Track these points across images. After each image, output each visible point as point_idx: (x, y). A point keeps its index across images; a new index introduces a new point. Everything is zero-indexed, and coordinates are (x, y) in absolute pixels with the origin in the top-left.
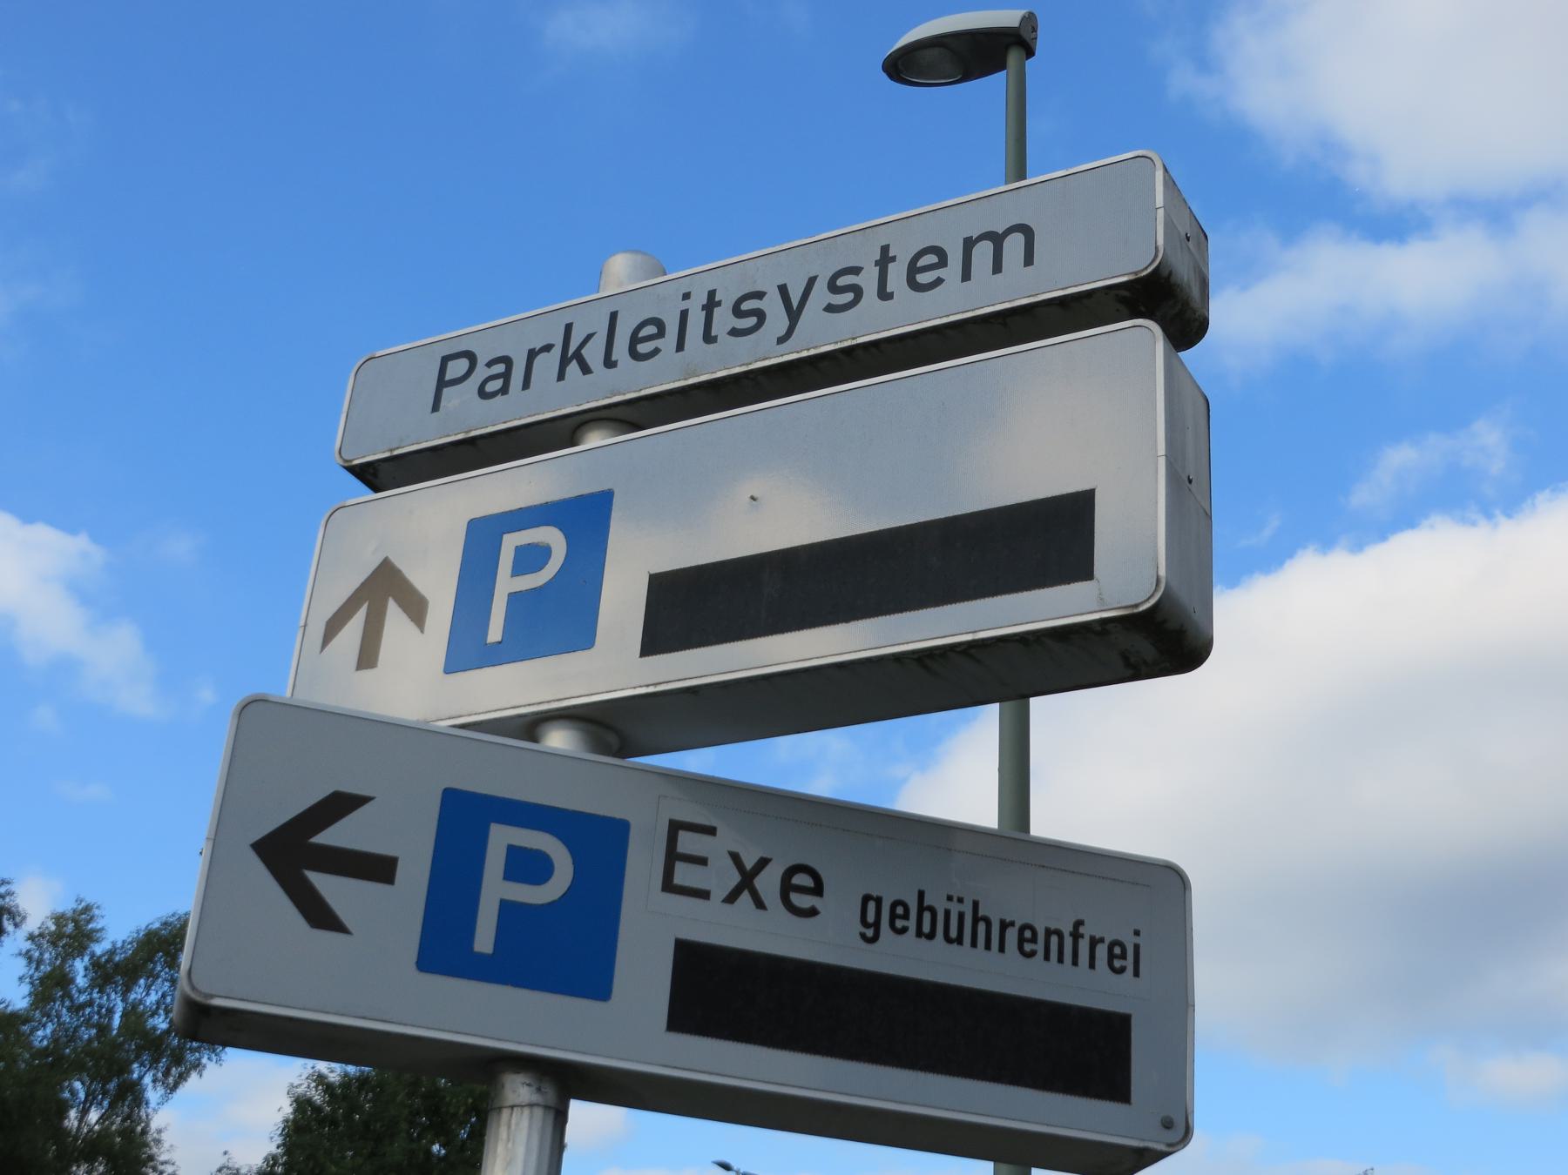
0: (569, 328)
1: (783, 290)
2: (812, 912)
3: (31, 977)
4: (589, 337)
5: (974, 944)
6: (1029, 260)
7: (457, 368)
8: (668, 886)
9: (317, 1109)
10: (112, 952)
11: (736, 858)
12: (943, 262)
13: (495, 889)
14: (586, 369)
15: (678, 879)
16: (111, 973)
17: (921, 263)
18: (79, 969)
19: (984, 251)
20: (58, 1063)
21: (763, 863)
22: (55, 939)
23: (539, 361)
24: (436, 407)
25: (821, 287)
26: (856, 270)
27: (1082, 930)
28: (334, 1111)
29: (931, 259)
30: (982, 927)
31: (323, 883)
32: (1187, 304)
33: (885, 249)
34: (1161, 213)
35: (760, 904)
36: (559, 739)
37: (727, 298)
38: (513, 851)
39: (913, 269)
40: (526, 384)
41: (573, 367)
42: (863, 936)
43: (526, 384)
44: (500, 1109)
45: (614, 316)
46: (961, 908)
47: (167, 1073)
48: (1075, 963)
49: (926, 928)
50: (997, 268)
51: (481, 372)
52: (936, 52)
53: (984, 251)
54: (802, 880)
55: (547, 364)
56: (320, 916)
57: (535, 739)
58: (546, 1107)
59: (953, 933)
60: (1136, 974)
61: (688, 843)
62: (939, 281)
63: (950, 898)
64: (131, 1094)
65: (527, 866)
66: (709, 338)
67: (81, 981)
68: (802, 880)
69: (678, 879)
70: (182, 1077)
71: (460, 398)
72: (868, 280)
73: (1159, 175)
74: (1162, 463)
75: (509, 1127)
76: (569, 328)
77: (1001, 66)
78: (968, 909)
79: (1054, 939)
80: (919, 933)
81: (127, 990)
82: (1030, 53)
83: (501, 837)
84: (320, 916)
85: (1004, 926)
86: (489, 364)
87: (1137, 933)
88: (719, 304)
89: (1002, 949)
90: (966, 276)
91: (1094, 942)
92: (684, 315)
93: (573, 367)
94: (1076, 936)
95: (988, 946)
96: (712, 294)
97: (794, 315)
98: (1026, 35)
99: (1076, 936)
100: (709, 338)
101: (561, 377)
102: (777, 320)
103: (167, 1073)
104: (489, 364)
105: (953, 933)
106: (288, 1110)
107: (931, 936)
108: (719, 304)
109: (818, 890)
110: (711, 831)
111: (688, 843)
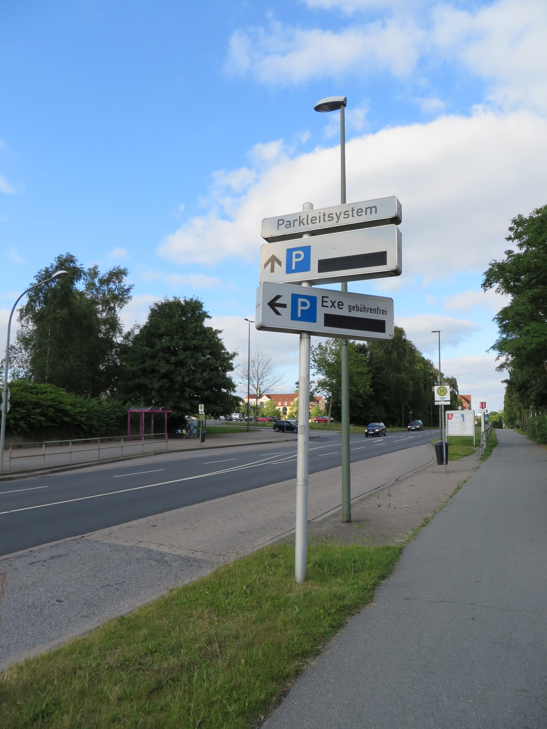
1: (336, 213)
2: (342, 308)
3: (85, 283)
4: (304, 219)
6: (376, 212)
7: (281, 222)
8: (323, 306)
9: (156, 311)
10: (103, 277)
11: (331, 301)
13: (300, 308)
14: (304, 225)
15: (324, 305)
18: (96, 281)
19: (369, 210)
21: (335, 301)
23: (296, 222)
25: (342, 214)
30: (365, 309)
35: (335, 308)
37: (327, 214)
38: (302, 302)
40: (294, 226)
43: (294, 226)
46: (362, 306)
49: (357, 310)
50: (371, 213)
51: (285, 223)
53: (369, 210)
54: (340, 304)
55: (297, 223)
56: (278, 313)
57: (301, 285)
61: (325, 299)
62: (362, 215)
65: (304, 304)
66: (324, 221)
68: (340, 304)
69: (324, 305)
71: (282, 227)
72: (350, 213)
73: (396, 200)
74: (397, 247)
77: (340, 108)
78: (363, 306)
79: (375, 310)
80: (357, 310)
81: (108, 285)
82: (345, 106)
83: (300, 300)
84: (278, 313)
85: (368, 308)
88: (325, 215)
89: (368, 312)
91: (380, 310)
92: (320, 216)
94: (378, 309)
96: (324, 213)
97: (338, 218)
98: (345, 103)
99: (378, 309)
100: (324, 221)
101: (300, 225)
102: (336, 219)
106: (150, 312)
107: (358, 311)
108: (325, 215)
109: (342, 305)
110: (328, 297)
111: (325, 299)
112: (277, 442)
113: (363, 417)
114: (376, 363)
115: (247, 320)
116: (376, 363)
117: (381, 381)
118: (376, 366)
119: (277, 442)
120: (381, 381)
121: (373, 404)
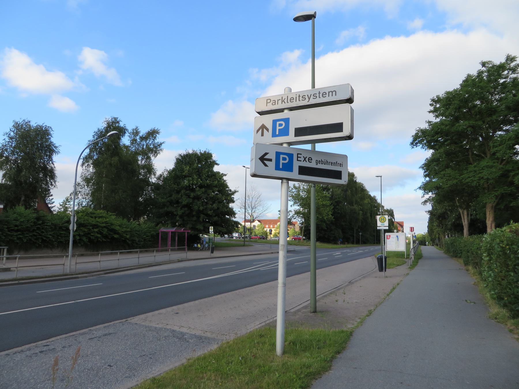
1: (308, 95)
2: (311, 162)
4: (285, 99)
7: (269, 101)
8: (298, 160)
9: (180, 160)
10: (143, 135)
11: (304, 157)
13: (282, 162)
14: (285, 103)
15: (298, 159)
16: (142, 138)
17: (324, 94)
19: (331, 93)
20: (137, 153)
21: (306, 157)
22: (133, 133)
23: (279, 101)
24: (267, 106)
25: (312, 96)
26: (316, 94)
28: (183, 160)
29: (325, 94)
30: (327, 163)
32: (352, 100)
35: (306, 162)
37: (301, 96)
38: (283, 158)
40: (278, 104)
41: (283, 102)
43: (278, 104)
47: (154, 155)
51: (272, 102)
52: (301, 18)
53: (331, 93)
54: (310, 159)
64: (149, 158)
66: (299, 100)
67: (138, 140)
68: (310, 159)
69: (298, 159)
70: (157, 155)
72: (318, 95)
73: (350, 86)
76: (282, 97)
78: (326, 161)
80: (321, 164)
82: (315, 18)
83: (282, 156)
84: (266, 165)
85: (330, 162)
86: (273, 101)
90: (329, 96)
91: (338, 164)
92: (296, 97)
93: (283, 102)
94: (336, 163)
95: (328, 165)
96: (299, 95)
97: (309, 99)
99: (336, 163)
100: (299, 100)
101: (282, 103)
102: (307, 99)
103: (154, 155)
104: (273, 101)
106: (175, 161)
107: (323, 164)
109: (312, 160)
110: (301, 154)
111: (299, 156)
114: (336, 199)
116: (336, 199)
117: (339, 211)
120: (339, 211)
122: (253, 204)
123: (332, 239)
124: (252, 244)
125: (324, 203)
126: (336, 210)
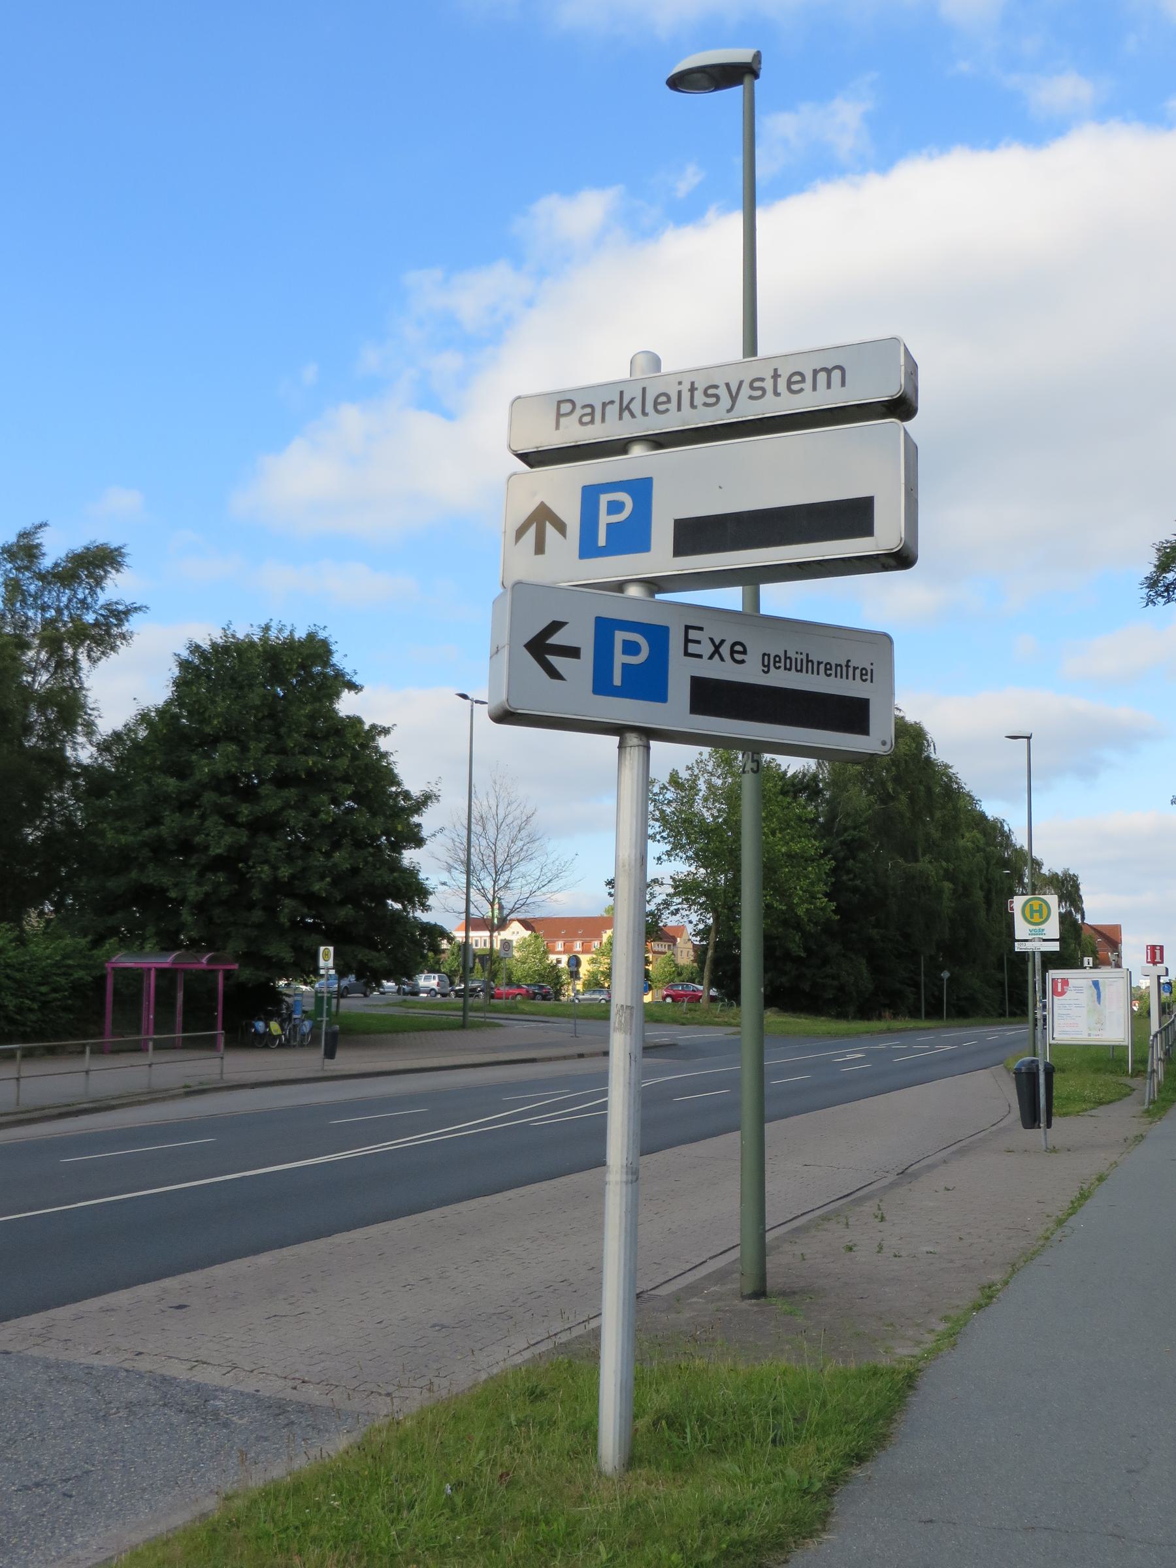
0: (622, 393)
1: (727, 385)
2: (742, 662)
4: (633, 399)
5: (807, 672)
6: (843, 384)
7: (566, 408)
8: (687, 654)
10: (56, 565)
11: (712, 640)
12: (803, 380)
14: (633, 416)
19: (822, 377)
21: (723, 641)
25: (745, 386)
27: (850, 664)
30: (810, 664)
31: (553, 659)
33: (776, 370)
34: (903, 368)
35: (722, 659)
36: (634, 591)
37: (701, 386)
39: (789, 383)
41: (626, 414)
42: (763, 671)
44: (625, 747)
45: (644, 390)
46: (801, 656)
48: (847, 678)
49: (788, 666)
50: (829, 386)
53: (822, 377)
54: (738, 648)
56: (554, 673)
58: (644, 746)
59: (799, 668)
60: (872, 681)
61: (693, 635)
63: (797, 653)
66: (693, 406)
68: (738, 648)
72: (768, 385)
73: (902, 348)
75: (630, 754)
80: (785, 669)
83: (620, 636)
84: (554, 673)
87: (872, 664)
88: (697, 389)
89: (818, 674)
91: (855, 669)
92: (680, 393)
93: (626, 414)
94: (847, 666)
95: (813, 673)
97: (734, 399)
98: (755, 67)
100: (693, 406)
102: (726, 401)
105: (799, 668)
107: (790, 669)
108: (697, 389)
109: (744, 652)
110: (701, 629)
111: (693, 635)
112: (550, 1059)
113: (806, 986)
115: (464, 697)
116: (846, 829)
118: (846, 836)
119: (550, 1059)
120: (858, 882)
121: (834, 949)
122: (499, 851)
123: (829, 995)
124: (488, 1020)
125: (796, 847)
126: (845, 878)
